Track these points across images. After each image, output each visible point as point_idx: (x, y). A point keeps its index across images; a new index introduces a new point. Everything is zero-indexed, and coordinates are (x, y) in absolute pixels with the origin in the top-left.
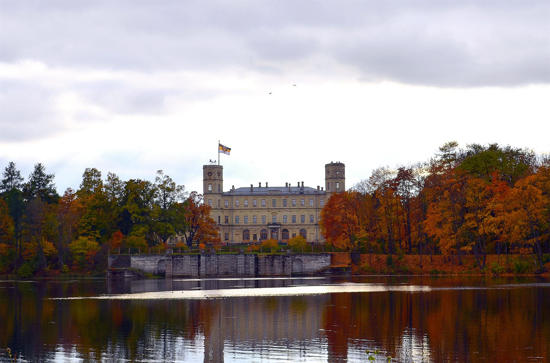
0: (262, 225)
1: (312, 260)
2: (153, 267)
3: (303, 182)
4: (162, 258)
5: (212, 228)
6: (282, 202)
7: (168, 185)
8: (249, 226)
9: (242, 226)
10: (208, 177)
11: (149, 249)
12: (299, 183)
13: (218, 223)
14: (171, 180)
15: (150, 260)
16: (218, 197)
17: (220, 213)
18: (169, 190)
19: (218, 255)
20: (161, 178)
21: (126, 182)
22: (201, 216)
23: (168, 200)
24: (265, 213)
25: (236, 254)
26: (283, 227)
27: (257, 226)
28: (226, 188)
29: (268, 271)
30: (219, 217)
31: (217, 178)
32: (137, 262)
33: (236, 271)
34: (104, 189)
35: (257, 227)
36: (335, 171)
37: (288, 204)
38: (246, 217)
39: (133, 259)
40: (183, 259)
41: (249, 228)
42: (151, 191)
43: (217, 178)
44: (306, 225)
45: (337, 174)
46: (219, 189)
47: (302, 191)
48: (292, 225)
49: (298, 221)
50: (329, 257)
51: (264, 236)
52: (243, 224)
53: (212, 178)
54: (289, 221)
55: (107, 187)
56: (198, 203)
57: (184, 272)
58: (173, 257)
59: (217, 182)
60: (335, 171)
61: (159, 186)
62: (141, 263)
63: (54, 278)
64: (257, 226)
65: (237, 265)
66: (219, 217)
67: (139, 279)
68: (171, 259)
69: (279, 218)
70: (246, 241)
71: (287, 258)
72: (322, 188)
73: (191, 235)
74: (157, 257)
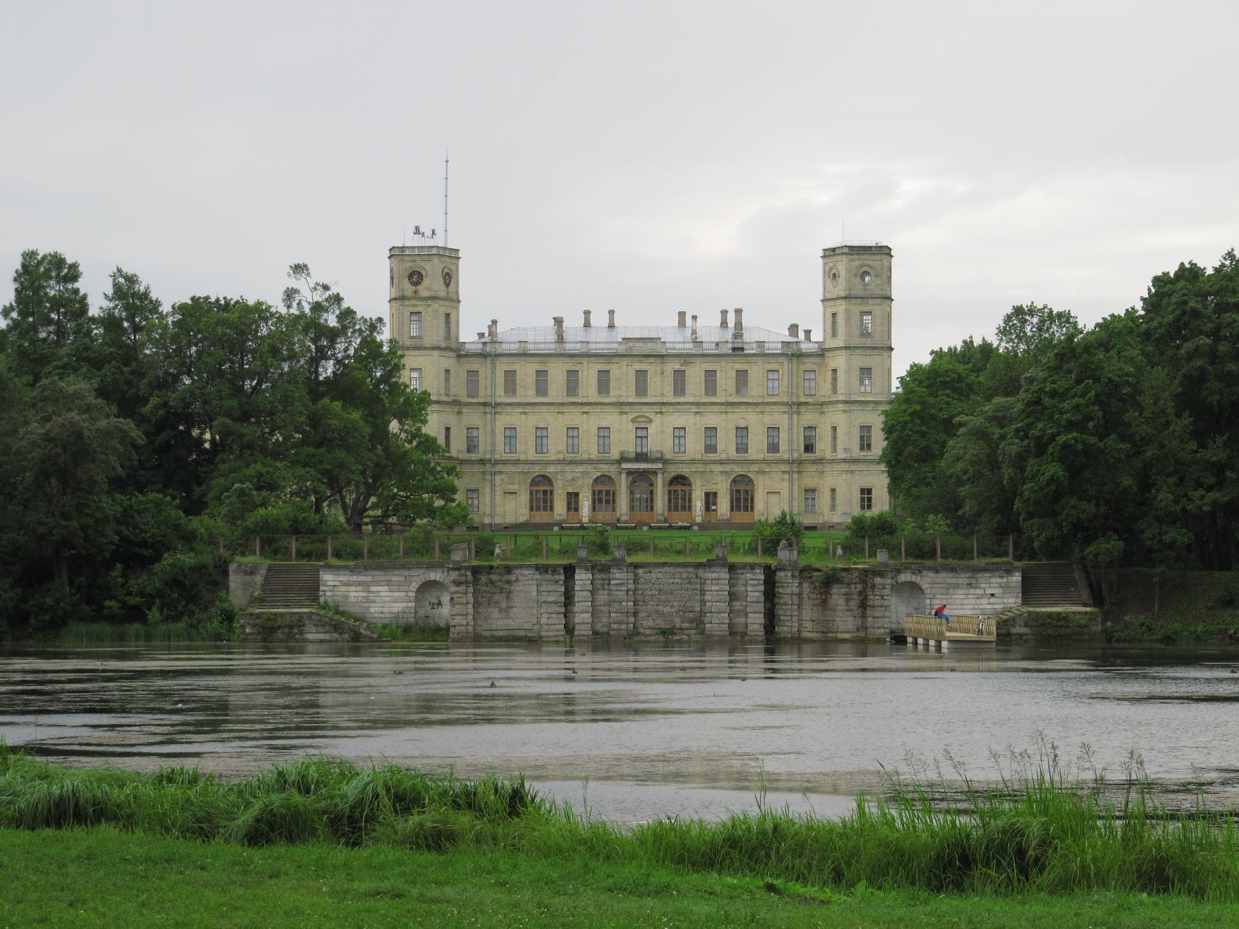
0: (599, 461)
1: (957, 586)
2: (397, 607)
3: (738, 312)
4: (435, 575)
6: (669, 380)
7: (332, 320)
8: (552, 463)
9: (526, 462)
10: (409, 289)
12: (724, 313)
14: (337, 299)
16: (448, 361)
17: (450, 418)
19: (636, 566)
24: (611, 419)
25: (699, 566)
26: (673, 470)
27: (581, 463)
28: (469, 333)
29: (809, 625)
30: (448, 429)
32: (339, 586)
33: (699, 622)
35: (580, 468)
36: (862, 273)
37: (652, 389)
38: (541, 433)
39: (328, 578)
40: (513, 578)
41: (551, 469)
44: (753, 462)
45: (865, 285)
48: (705, 463)
49: (726, 445)
50: (1017, 578)
51: (604, 496)
52: (532, 455)
53: (423, 291)
54: (694, 446)
55: (110, 322)
57: (513, 624)
58: (476, 571)
62: (355, 594)
63: (1050, 632)
64: (581, 463)
65: (703, 603)
66: (448, 429)
67: (356, 652)
69: (659, 439)
70: (541, 517)
71: (878, 580)
72: (808, 332)
74: (414, 572)
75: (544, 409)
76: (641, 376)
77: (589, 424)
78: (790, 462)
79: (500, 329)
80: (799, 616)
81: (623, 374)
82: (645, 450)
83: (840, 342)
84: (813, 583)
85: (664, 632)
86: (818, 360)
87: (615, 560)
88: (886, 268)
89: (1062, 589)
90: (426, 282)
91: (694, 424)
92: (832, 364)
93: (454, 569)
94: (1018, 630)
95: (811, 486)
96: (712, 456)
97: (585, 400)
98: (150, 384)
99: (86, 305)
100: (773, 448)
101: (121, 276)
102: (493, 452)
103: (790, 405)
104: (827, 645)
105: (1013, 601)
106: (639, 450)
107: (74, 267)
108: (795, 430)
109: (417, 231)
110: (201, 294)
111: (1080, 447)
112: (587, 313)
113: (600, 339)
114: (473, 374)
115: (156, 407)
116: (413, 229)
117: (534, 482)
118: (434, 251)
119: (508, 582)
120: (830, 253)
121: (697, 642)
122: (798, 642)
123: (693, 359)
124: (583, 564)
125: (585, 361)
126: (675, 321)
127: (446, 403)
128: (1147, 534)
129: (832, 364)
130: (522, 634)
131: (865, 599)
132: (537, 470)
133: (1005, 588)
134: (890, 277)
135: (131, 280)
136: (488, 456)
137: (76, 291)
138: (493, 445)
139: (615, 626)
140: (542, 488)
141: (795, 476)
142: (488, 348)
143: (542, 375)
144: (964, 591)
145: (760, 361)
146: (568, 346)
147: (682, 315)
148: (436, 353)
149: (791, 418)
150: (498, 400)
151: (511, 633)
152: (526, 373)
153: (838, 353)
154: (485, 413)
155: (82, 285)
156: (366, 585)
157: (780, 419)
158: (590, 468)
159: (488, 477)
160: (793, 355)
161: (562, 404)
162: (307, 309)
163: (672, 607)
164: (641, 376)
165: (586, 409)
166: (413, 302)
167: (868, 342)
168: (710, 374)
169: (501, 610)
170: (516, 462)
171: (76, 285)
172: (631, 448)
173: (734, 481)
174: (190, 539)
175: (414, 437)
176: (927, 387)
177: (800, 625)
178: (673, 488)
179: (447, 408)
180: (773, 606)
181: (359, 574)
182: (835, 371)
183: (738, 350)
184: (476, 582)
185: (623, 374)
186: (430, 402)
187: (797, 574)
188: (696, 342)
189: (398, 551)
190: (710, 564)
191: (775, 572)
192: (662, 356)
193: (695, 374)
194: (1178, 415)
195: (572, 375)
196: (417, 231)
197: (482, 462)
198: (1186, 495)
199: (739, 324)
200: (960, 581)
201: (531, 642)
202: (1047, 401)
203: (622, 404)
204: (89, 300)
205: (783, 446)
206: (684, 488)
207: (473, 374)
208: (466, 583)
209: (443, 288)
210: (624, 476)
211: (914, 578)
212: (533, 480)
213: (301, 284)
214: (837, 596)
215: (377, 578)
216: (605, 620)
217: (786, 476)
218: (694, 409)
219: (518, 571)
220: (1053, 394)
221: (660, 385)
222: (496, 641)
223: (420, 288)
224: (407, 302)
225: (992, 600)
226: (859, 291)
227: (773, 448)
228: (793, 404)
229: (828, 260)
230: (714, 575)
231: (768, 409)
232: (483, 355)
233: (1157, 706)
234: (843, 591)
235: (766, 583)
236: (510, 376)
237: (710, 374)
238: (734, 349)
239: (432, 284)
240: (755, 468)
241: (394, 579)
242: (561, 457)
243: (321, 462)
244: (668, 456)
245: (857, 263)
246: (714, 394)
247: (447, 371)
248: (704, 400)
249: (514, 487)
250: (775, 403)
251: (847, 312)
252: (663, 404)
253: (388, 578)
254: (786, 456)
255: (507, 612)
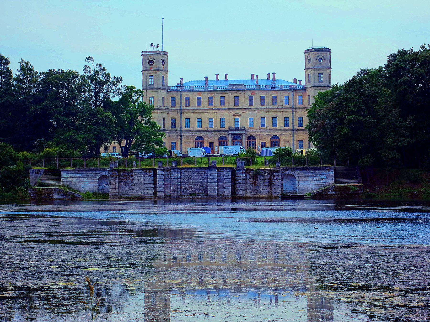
0: (221, 131)
1: (309, 176)
2: (91, 186)
4: (105, 173)
5: (155, 135)
7: (101, 77)
8: (203, 131)
9: (194, 131)
10: (149, 67)
11: (87, 159)
12: (269, 74)
13: (162, 128)
14: (104, 69)
15: (87, 176)
16: (163, 94)
17: (164, 115)
18: (102, 83)
19: (181, 169)
20: (92, 67)
21: (43, 73)
22: (139, 119)
23: (101, 95)
24: (225, 115)
26: (249, 134)
27: (214, 131)
28: (172, 82)
29: (249, 192)
30: (164, 119)
31: (161, 67)
32: (69, 178)
33: (206, 190)
34: (15, 83)
35: (214, 133)
36: (319, 58)
38: (199, 120)
39: (64, 175)
40: (133, 174)
41: (203, 134)
42: (18, 82)
43: (161, 67)
46: (164, 83)
47: (273, 86)
48: (261, 131)
49: (269, 124)
50: (332, 172)
52: (195, 128)
54: (257, 124)
55: (18, 80)
56: (136, 101)
58: (119, 171)
59: (161, 74)
60: (319, 58)
61: (89, 77)
62: (75, 181)
64: (214, 131)
65: (207, 183)
66: (164, 119)
68: (117, 174)
69: (244, 123)
71: (276, 174)
72: (300, 81)
73: (127, 144)
75: (200, 111)
76: (237, 98)
77: (216, 117)
78: (293, 130)
79: (185, 81)
80: (246, 188)
81: (230, 98)
82: (238, 126)
83: (311, 85)
84: (250, 175)
85: (191, 194)
86: (303, 92)
87: (173, 166)
88: (328, 57)
89: (351, 177)
90: (155, 64)
91: (257, 117)
92: (308, 93)
93: (110, 171)
94: (330, 192)
95: (301, 139)
96: (263, 128)
97: (215, 108)
98: (31, 102)
99: (11, 73)
100: (287, 125)
101: (23, 62)
102: (181, 127)
103: (293, 109)
104: (256, 198)
105: (330, 182)
106: (236, 126)
107: (7, 59)
108: (295, 118)
109: (152, 45)
110: (52, 68)
111: (356, 120)
112: (217, 75)
113: (222, 85)
114: (173, 99)
115: (33, 111)
116: (150, 45)
117: (196, 139)
118: (158, 52)
119: (132, 175)
120: (307, 51)
121: (204, 198)
122: (245, 198)
123: (256, 92)
124: (160, 168)
125: (215, 93)
126: (250, 78)
127: (163, 109)
128: (383, 155)
129: (308, 93)
130: (137, 196)
131: (271, 181)
132: (198, 134)
133: (328, 176)
134: (330, 60)
135: (27, 64)
136: (179, 129)
137: (8, 68)
138: (181, 125)
139: (173, 192)
140: (199, 141)
141: (295, 135)
142: (179, 89)
143: (199, 98)
144: (311, 178)
145: (281, 92)
146: (209, 88)
147: (253, 75)
148: (159, 91)
149: (293, 114)
150: (183, 108)
151: (133, 195)
152: (193, 98)
153: (311, 89)
154: (178, 113)
155: (10, 67)
156: (79, 177)
157: (289, 114)
158: (218, 133)
159: (179, 137)
160: (293, 90)
161: (207, 109)
162: (92, 73)
163: (195, 185)
164: (237, 98)
165: (216, 111)
166: (150, 72)
167: (322, 85)
168: (263, 98)
169: (129, 187)
170: (190, 131)
171: (8, 66)
172: (233, 126)
173: (272, 138)
174: (15, 160)
175: (148, 122)
176: (324, 100)
177: (246, 191)
178: (249, 140)
179: (163, 111)
180: (235, 184)
181: (76, 173)
182: (309, 96)
183: (273, 88)
184: (119, 175)
185: (230, 98)
186: (153, 109)
187: (244, 171)
188: (257, 85)
189: (97, 164)
190: (210, 168)
191: (235, 171)
192: (244, 91)
193: (257, 98)
194: (395, 108)
195: (211, 99)
196: (152, 45)
197: (177, 131)
198: (398, 140)
199: (274, 78)
200: (310, 174)
201: (140, 198)
202: (344, 103)
203: (229, 109)
204: (12, 72)
205: (290, 124)
206: (253, 140)
207: (173, 99)
208: (116, 176)
209: (162, 66)
210: (230, 136)
211: (292, 173)
212: (196, 138)
213: (89, 64)
214: (260, 180)
215: (83, 175)
216: (169, 190)
217: (292, 136)
218: (256, 111)
219: (136, 171)
220: (347, 100)
221: (244, 102)
222: (127, 198)
223: (152, 66)
224: (148, 72)
225: (322, 181)
226: (318, 65)
227: (287, 125)
228: (294, 108)
229: (306, 54)
230: (211, 172)
231: (285, 110)
232: (177, 91)
233: (310, 224)
234: (263, 178)
235: (232, 175)
236: (187, 99)
237: (263, 98)
238: (271, 88)
239: (158, 65)
240: (280, 132)
241: (89, 175)
242: (206, 129)
243: (95, 131)
244: (247, 129)
245: (317, 55)
246: (264, 105)
247: (163, 98)
248: (260, 107)
249: (189, 141)
250: (287, 108)
251: (314, 73)
252: (244, 109)
253: (87, 174)
254: (291, 128)
255: (131, 187)
